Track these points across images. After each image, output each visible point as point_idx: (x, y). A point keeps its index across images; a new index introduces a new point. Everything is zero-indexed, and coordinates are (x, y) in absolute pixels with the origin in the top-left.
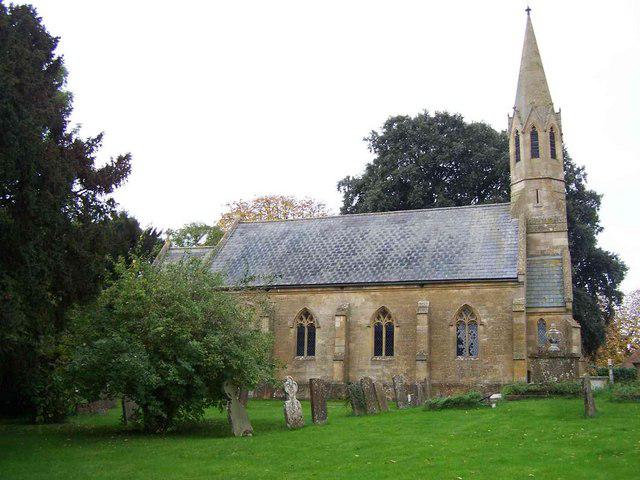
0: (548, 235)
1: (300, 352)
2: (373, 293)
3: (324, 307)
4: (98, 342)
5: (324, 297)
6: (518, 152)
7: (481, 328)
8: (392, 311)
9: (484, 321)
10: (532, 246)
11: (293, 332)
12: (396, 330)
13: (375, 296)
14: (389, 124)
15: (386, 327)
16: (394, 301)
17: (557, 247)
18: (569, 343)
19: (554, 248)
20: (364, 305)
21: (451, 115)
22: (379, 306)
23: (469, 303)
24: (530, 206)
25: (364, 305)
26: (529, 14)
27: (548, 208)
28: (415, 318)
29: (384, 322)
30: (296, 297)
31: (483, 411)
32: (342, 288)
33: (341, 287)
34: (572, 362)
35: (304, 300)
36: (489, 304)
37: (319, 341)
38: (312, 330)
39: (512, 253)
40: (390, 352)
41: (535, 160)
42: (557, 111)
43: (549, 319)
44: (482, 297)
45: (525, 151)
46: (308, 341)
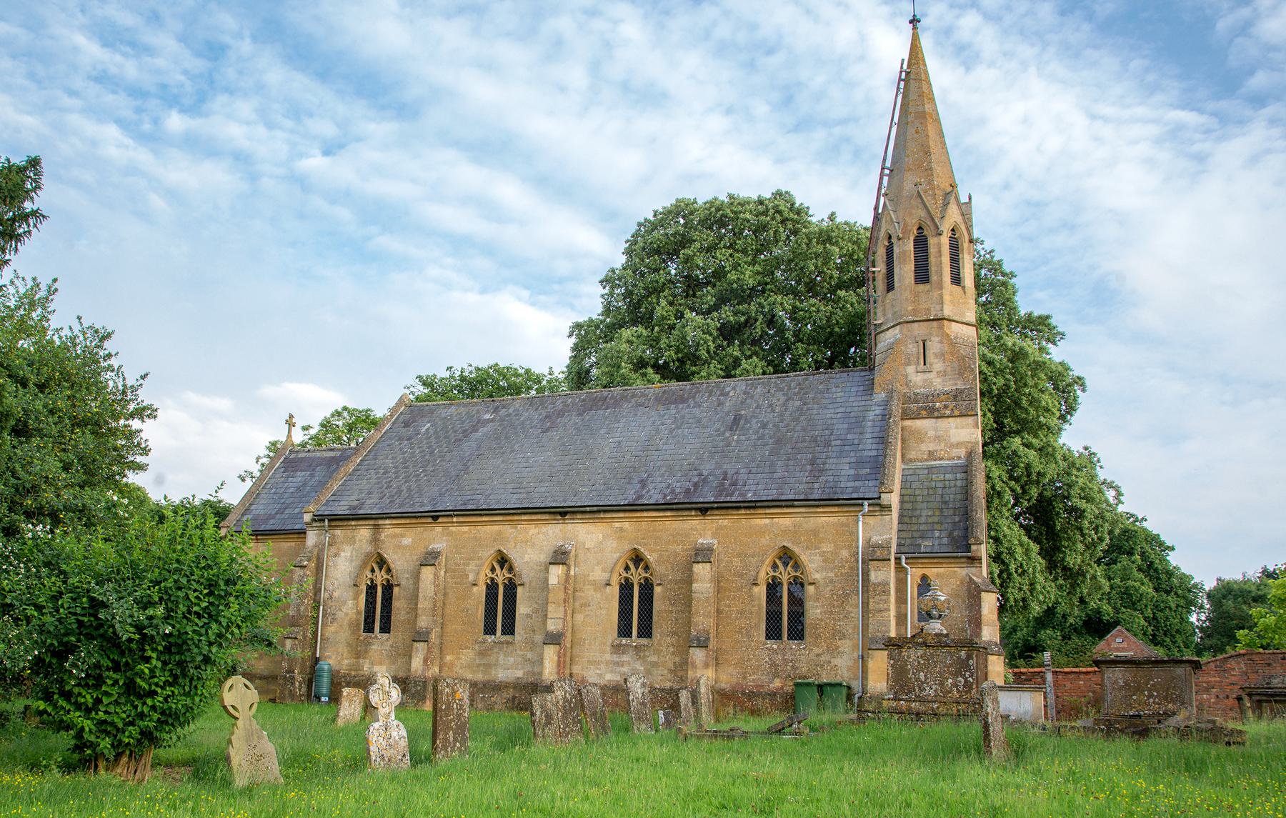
0: (942, 424)
1: (490, 629)
2: (617, 525)
3: (530, 544)
4: (90, 127)
5: (533, 530)
6: (890, 274)
7: (810, 589)
8: (650, 557)
9: (817, 576)
10: (912, 443)
11: (480, 591)
12: (658, 590)
13: (621, 529)
14: (778, 194)
15: (641, 585)
16: (666, 538)
17: (958, 445)
18: (976, 622)
19: (952, 446)
20: (599, 546)
21: (620, 260)
22: (627, 547)
23: (789, 545)
24: (910, 370)
25: (599, 546)
26: (914, 28)
27: (943, 374)
28: (690, 570)
29: (636, 576)
30: (489, 533)
31: (398, 531)
32: (563, 514)
33: (562, 513)
34: (969, 657)
35: (498, 537)
36: (827, 547)
37: (522, 609)
38: (511, 588)
39: (874, 453)
40: (646, 631)
41: (921, 287)
42: (964, 199)
43: (938, 575)
44: (815, 532)
45: (905, 271)
46: (496, 604)
